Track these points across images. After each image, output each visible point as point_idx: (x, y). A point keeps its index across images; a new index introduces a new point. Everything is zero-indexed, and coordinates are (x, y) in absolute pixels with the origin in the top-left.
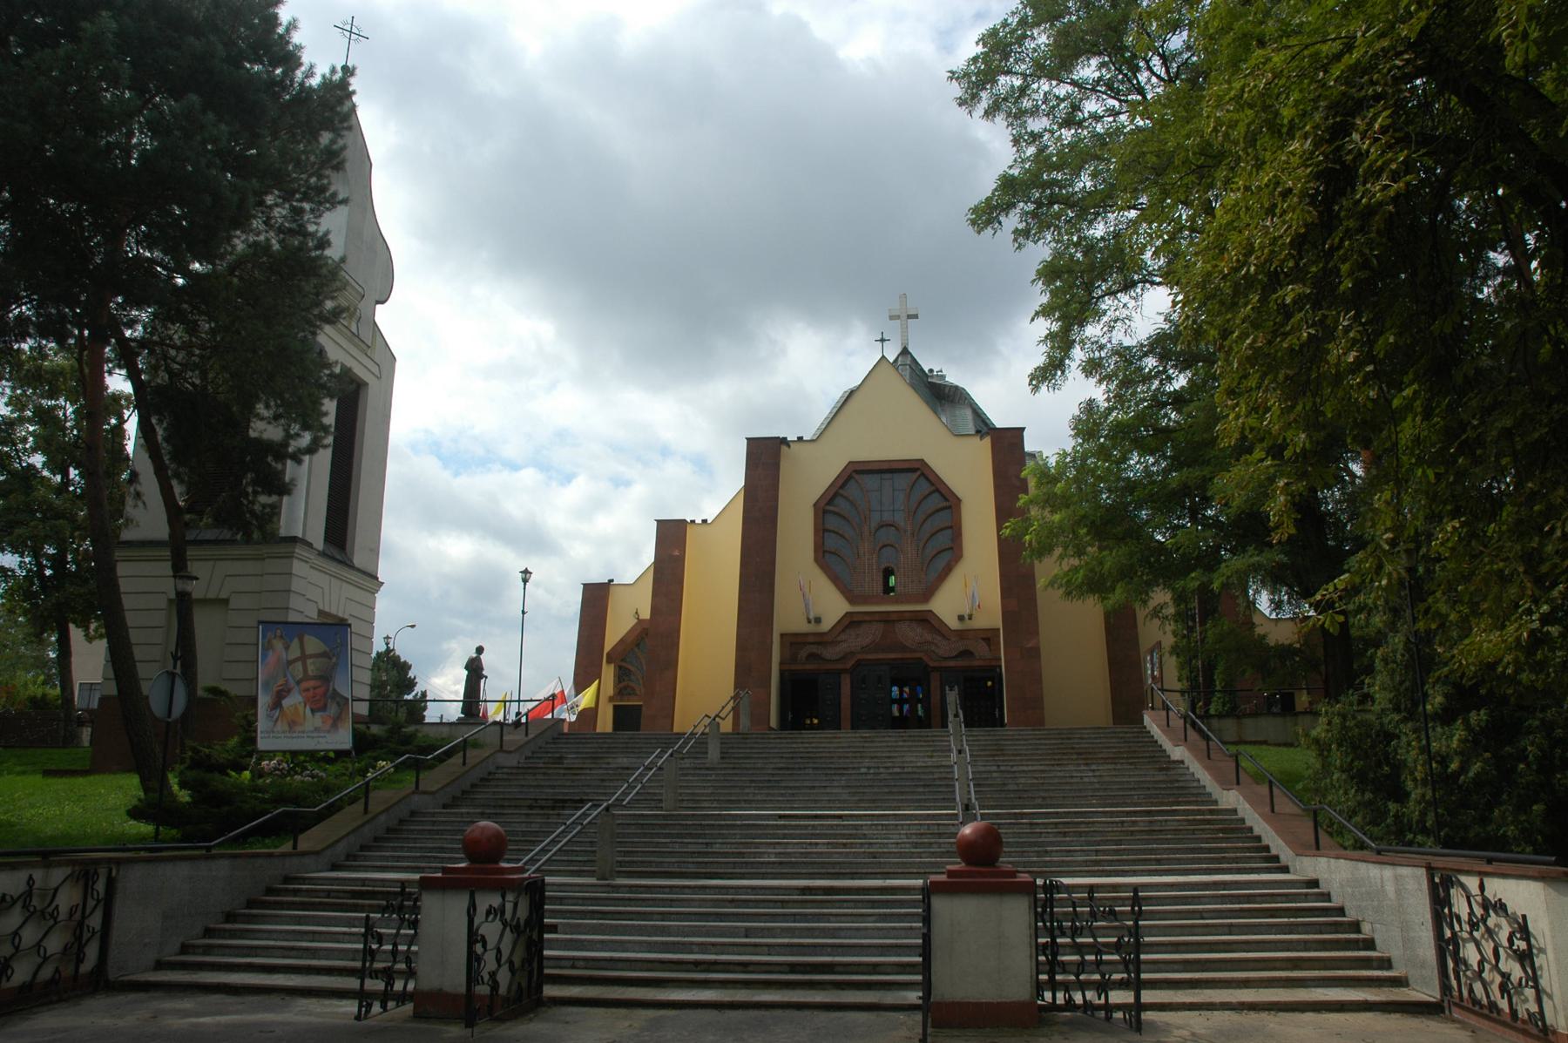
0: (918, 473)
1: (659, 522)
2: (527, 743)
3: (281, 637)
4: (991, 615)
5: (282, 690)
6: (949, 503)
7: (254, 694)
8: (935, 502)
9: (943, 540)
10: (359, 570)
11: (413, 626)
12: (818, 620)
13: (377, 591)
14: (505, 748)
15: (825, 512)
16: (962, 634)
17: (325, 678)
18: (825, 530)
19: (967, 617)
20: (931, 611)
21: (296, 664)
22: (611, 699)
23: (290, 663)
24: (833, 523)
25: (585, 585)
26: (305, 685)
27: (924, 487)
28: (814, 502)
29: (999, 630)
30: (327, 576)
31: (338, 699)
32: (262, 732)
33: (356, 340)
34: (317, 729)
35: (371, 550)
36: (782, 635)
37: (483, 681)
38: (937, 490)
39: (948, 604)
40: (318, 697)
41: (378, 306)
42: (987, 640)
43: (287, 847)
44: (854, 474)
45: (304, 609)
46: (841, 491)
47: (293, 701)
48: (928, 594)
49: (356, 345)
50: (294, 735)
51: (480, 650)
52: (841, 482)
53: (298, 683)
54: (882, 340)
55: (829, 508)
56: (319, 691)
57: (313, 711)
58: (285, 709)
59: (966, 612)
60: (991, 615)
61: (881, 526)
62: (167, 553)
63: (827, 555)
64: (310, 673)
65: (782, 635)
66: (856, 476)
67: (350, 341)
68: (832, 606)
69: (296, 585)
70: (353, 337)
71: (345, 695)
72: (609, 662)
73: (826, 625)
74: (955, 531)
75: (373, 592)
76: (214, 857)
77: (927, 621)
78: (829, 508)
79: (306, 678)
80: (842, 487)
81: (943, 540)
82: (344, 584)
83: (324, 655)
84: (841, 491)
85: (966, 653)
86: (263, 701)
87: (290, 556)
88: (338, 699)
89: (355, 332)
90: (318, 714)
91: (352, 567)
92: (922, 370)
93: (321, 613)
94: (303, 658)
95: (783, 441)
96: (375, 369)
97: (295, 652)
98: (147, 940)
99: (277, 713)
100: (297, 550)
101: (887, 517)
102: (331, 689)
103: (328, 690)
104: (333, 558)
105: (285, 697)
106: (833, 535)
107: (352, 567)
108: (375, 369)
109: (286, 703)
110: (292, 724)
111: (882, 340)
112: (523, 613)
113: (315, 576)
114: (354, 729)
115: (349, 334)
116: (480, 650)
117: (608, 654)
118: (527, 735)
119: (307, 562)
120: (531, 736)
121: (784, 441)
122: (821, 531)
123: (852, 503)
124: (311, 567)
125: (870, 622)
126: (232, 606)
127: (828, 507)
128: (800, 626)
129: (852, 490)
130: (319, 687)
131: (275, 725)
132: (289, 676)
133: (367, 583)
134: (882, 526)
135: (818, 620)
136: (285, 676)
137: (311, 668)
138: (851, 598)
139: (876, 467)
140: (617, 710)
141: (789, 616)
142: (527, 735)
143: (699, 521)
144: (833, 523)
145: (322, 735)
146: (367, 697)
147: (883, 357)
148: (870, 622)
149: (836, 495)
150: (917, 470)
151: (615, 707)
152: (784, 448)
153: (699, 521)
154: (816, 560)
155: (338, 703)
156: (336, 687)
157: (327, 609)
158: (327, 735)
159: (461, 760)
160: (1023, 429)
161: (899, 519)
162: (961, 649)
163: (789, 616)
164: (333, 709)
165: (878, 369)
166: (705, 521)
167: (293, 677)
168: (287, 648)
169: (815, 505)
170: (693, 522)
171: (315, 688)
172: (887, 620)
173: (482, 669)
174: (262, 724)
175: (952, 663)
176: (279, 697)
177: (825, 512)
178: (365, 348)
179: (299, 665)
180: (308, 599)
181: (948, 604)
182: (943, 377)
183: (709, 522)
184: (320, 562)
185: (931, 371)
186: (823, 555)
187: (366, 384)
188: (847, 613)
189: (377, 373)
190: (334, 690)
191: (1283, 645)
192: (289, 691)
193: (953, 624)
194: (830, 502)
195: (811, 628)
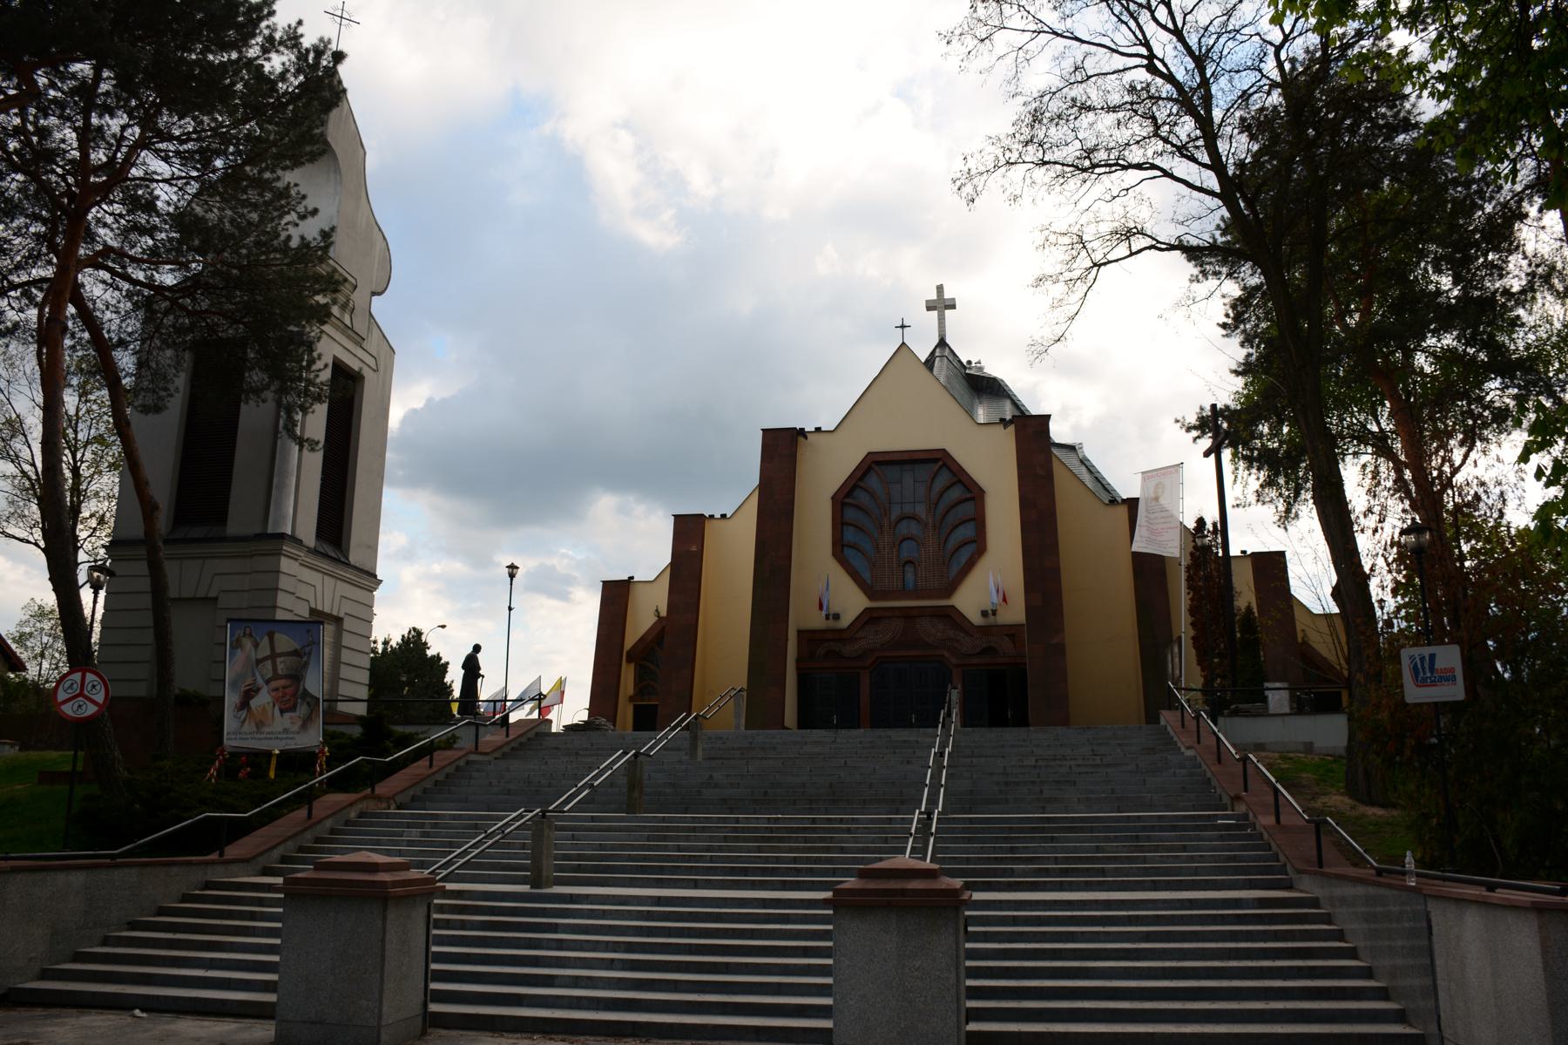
0: (940, 463)
1: (676, 517)
2: (508, 743)
3: (251, 635)
4: (1015, 613)
5: (249, 690)
6: (974, 494)
7: (221, 694)
8: (956, 493)
9: (966, 531)
10: (355, 568)
11: (443, 627)
12: (837, 617)
13: (375, 589)
14: (480, 749)
15: (843, 505)
16: (985, 630)
17: (296, 677)
18: (843, 524)
19: (990, 612)
20: (953, 606)
21: (266, 663)
22: (631, 699)
23: (259, 662)
24: (850, 514)
25: (605, 583)
26: (274, 684)
27: (943, 479)
28: (831, 495)
29: (1452, 670)
30: (321, 575)
33: (350, 332)
34: (286, 731)
35: (369, 547)
36: (800, 632)
37: (480, 680)
38: (960, 481)
39: (972, 598)
40: (288, 697)
41: (375, 299)
42: (1011, 636)
43: (214, 856)
44: (873, 465)
45: (290, 606)
46: (861, 484)
47: (263, 699)
48: (951, 588)
49: (349, 337)
50: (262, 736)
51: (477, 648)
52: (859, 474)
53: (267, 682)
54: (903, 327)
55: (846, 500)
56: (289, 690)
57: (282, 712)
58: (253, 709)
59: (989, 608)
60: (1015, 613)
61: (901, 519)
62: (142, 551)
63: (846, 549)
64: (280, 672)
65: (800, 632)
66: (876, 468)
67: (343, 333)
68: (850, 602)
69: (284, 582)
70: (346, 330)
71: (317, 695)
72: (629, 661)
73: (846, 621)
74: (979, 521)
75: (371, 590)
76: (117, 866)
77: (952, 617)
78: (846, 500)
79: (276, 676)
80: (861, 478)
81: (966, 531)
82: (339, 582)
83: (296, 653)
84: (861, 484)
85: (990, 650)
86: (231, 699)
87: (278, 553)
88: (309, 699)
89: (349, 324)
90: (287, 715)
92: (960, 362)
93: (313, 611)
94: (273, 656)
95: (801, 432)
96: (371, 362)
97: (264, 650)
98: (33, 955)
99: (243, 714)
100: (284, 548)
101: (908, 509)
102: (301, 688)
104: (325, 556)
105: (253, 697)
106: (851, 528)
107: (348, 565)
108: (371, 362)
109: (254, 703)
110: (260, 724)
111: (903, 327)
112: (510, 609)
113: (307, 575)
115: (342, 326)
116: (477, 648)
117: (628, 653)
118: (507, 735)
119: (296, 560)
120: (511, 737)
121: (802, 432)
122: (839, 524)
123: (872, 495)
124: (301, 564)
125: (890, 617)
127: (844, 499)
128: (817, 621)
129: (873, 481)
130: (290, 686)
131: (241, 726)
133: (365, 582)
134: (903, 519)
135: (837, 617)
136: (254, 675)
137: (281, 668)
138: (870, 592)
139: (896, 457)
140: (637, 709)
141: (803, 614)
142: (507, 735)
143: (718, 516)
144: (850, 514)
145: (291, 736)
146: (365, 697)
147: (903, 343)
148: (890, 617)
149: (855, 487)
150: (939, 461)
151: (636, 707)
152: (801, 439)
153: (718, 516)
154: (834, 554)
155: (308, 703)
156: (306, 687)
158: (296, 736)
159: (428, 763)
160: (1049, 416)
161: (921, 510)
162: (985, 645)
163: (803, 614)
164: (303, 710)
165: (897, 355)
166: (723, 516)
167: (262, 676)
168: (256, 646)
169: (832, 498)
170: (712, 517)
171: (285, 687)
172: (907, 615)
173: (479, 668)
174: (229, 723)
175: (975, 661)
176: (249, 695)
177: (843, 505)
178: (359, 339)
179: (269, 664)
180: (298, 598)
181: (972, 598)
182: (981, 369)
183: (728, 516)
184: (310, 560)
185: (969, 362)
186: (840, 549)
188: (866, 609)
190: (305, 690)
191: (152, 497)
192: (258, 690)
193: (975, 618)
194: (849, 495)
195: (831, 624)
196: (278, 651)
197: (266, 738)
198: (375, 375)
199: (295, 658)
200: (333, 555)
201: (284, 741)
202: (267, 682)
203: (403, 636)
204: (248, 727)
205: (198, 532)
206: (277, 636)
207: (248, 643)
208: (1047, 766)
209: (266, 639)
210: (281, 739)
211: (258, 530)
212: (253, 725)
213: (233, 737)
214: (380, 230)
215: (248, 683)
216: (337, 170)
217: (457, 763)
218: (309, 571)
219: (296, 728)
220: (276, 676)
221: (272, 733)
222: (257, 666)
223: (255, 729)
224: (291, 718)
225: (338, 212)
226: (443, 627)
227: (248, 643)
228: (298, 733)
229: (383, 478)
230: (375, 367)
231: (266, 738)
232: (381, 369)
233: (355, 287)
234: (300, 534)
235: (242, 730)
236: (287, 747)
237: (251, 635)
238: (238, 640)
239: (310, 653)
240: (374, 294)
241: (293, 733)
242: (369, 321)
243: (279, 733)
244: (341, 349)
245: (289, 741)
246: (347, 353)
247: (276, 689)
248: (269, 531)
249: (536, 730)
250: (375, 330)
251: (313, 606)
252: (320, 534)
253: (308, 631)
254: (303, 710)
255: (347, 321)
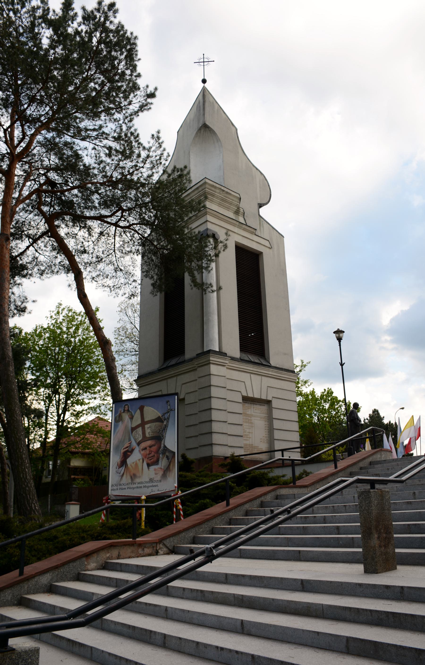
5: (127, 451)
11: (403, 408)
21: (138, 429)
23: (133, 429)
26: (143, 445)
30: (249, 375)
31: (167, 454)
32: (112, 486)
40: (153, 454)
49: (244, 230)
53: (139, 444)
56: (154, 448)
57: (149, 465)
58: (129, 465)
64: (147, 435)
67: (240, 228)
69: (214, 381)
70: (241, 225)
71: (173, 450)
79: (145, 439)
82: (263, 377)
83: (159, 420)
89: (244, 222)
90: (152, 468)
91: (270, 366)
94: (143, 424)
96: (267, 244)
97: (137, 420)
99: (123, 469)
100: (211, 359)
102: (162, 446)
103: (160, 447)
105: (129, 456)
107: (270, 366)
108: (267, 244)
109: (130, 461)
110: (133, 477)
112: (342, 365)
114: (179, 476)
115: (238, 223)
126: (186, 402)
132: (133, 440)
136: (130, 440)
145: (154, 484)
155: (167, 457)
156: (166, 444)
157: (250, 395)
164: (163, 463)
167: (135, 440)
168: (132, 418)
171: (150, 447)
176: (126, 455)
178: (253, 230)
179: (140, 430)
187: (261, 253)
189: (268, 245)
190: (165, 446)
192: (132, 451)
196: (146, 419)
197: (137, 487)
198: (271, 250)
199: (157, 423)
200: (257, 361)
201: (150, 489)
202: (139, 444)
203: (370, 415)
204: (126, 479)
205: (173, 362)
206: (146, 409)
207: (126, 417)
208: (41, 526)
209: (138, 411)
210: (148, 487)
211: (199, 351)
212: (129, 477)
213: (115, 488)
214: (257, 169)
215: (125, 446)
216: (218, 140)
217: (262, 499)
218: (237, 372)
219: (158, 477)
220: (145, 439)
221: (142, 483)
222: (132, 432)
223: (130, 481)
224: (155, 470)
225: (223, 161)
226: (403, 408)
227: (126, 417)
228: (160, 481)
229: (289, 311)
230: (270, 246)
231: (137, 487)
232: (275, 246)
233: (240, 199)
234: (225, 350)
235: (121, 483)
236: (152, 493)
237: (128, 411)
238: (120, 416)
239: (168, 418)
240: (260, 206)
241: (157, 481)
242: (260, 220)
243: (147, 482)
244: (240, 237)
245: (154, 489)
246: (246, 239)
247: (145, 449)
248: (205, 350)
249: (370, 459)
250: (265, 225)
251: (245, 394)
252: (243, 348)
253: (167, 402)
254: (163, 463)
255: (241, 220)
